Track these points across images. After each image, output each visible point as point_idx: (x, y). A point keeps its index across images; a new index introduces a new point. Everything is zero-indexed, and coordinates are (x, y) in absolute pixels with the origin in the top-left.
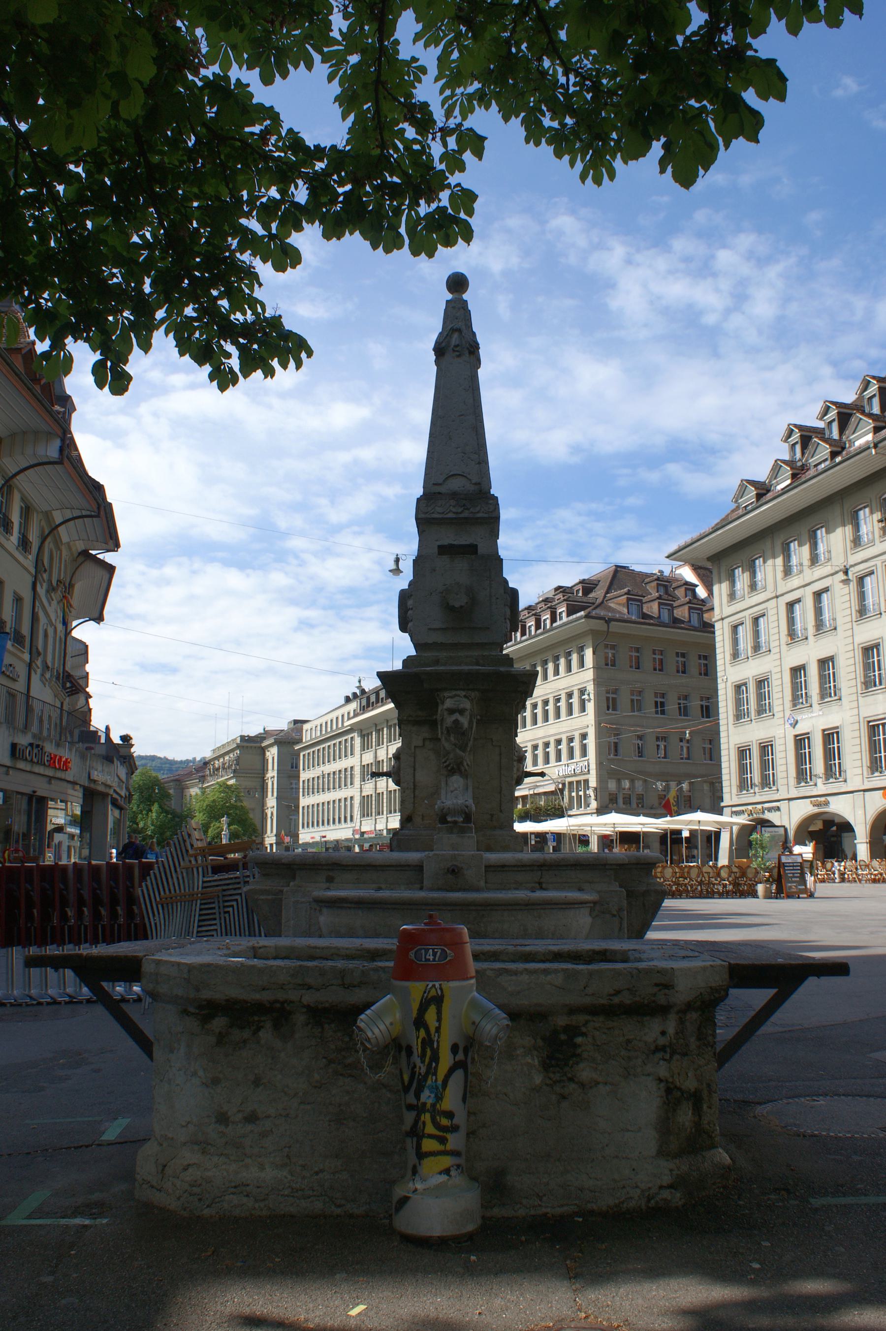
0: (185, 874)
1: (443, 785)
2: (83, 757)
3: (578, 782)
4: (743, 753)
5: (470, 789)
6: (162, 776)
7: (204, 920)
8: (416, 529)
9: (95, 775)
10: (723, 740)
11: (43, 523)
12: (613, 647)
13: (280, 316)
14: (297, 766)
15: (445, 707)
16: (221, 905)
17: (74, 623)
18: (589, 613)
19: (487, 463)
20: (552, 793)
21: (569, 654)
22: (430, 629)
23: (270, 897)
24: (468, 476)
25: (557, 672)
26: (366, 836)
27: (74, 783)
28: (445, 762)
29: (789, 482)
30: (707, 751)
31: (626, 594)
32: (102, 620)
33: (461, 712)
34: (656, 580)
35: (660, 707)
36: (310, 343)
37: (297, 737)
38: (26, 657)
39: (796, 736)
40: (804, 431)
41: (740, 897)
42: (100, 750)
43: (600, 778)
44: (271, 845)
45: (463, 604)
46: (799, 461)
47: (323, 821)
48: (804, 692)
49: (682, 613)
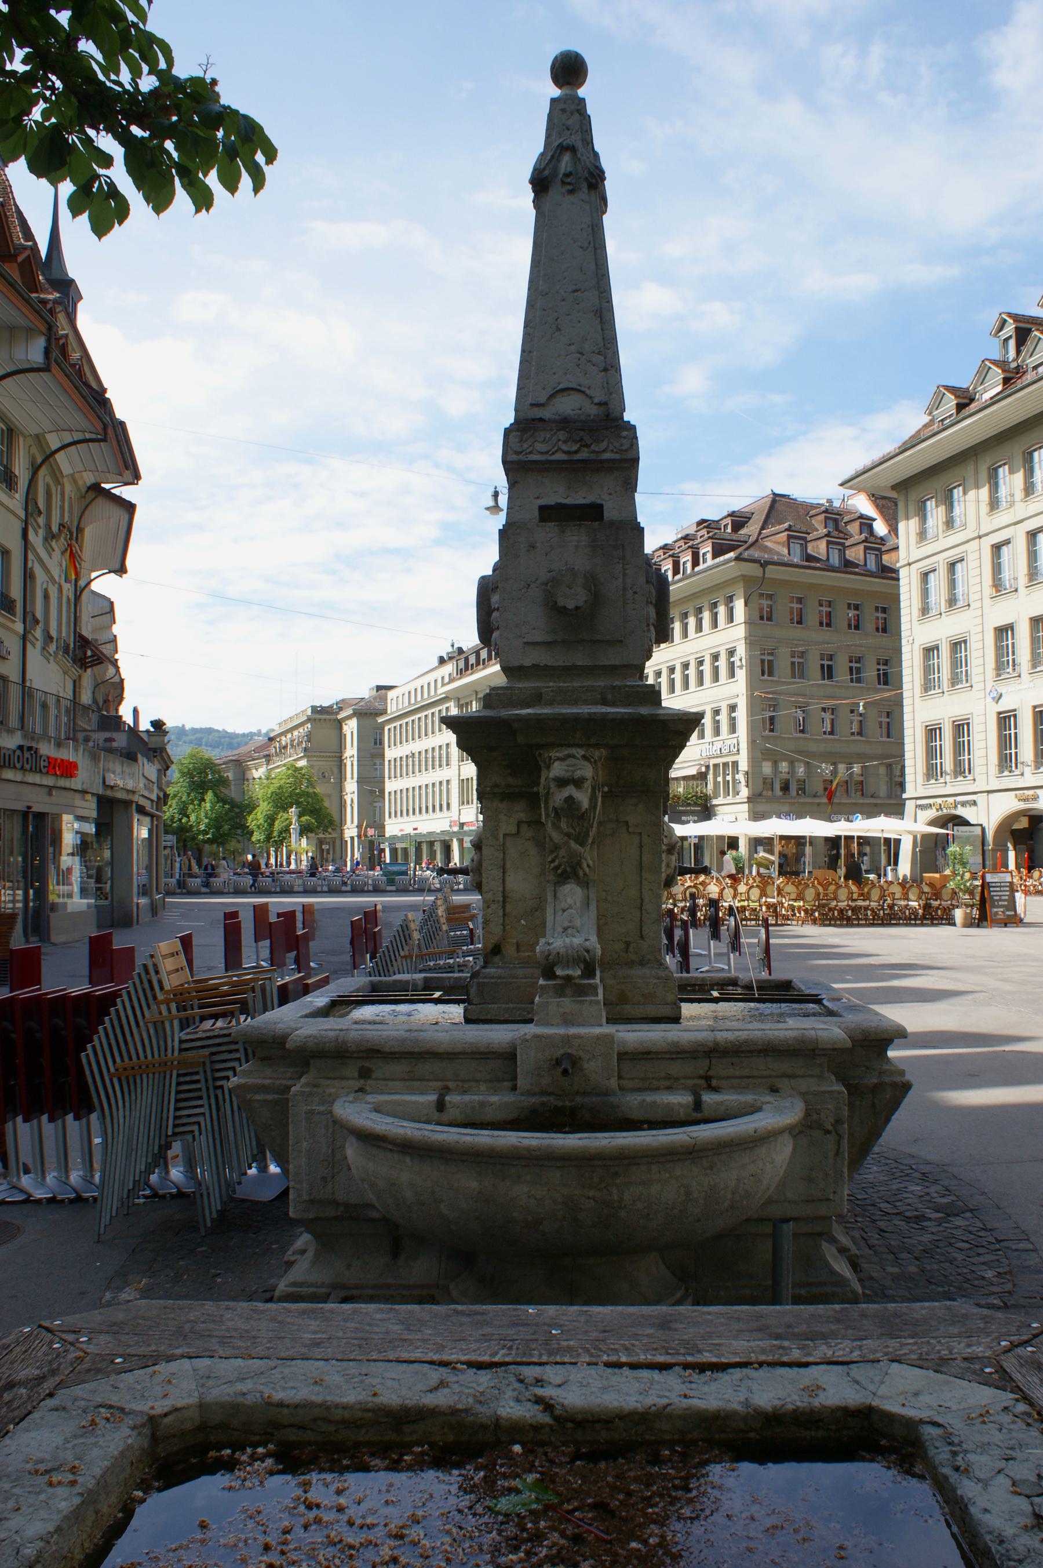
0: (152, 1031)
1: (550, 898)
2: (94, 757)
3: (726, 765)
4: (932, 732)
5: (593, 907)
6: (216, 755)
7: (185, 1100)
8: (505, 478)
9: (112, 779)
10: (907, 717)
11: (34, 450)
12: (770, 597)
13: (214, 82)
14: (381, 743)
15: (551, 775)
16: (210, 1077)
17: (94, 575)
18: (741, 554)
19: (618, 370)
20: (693, 777)
21: (715, 605)
22: (525, 643)
23: (270, 1097)
24: (588, 392)
25: (699, 628)
26: (466, 828)
27: (84, 792)
28: (553, 861)
29: (999, 388)
30: (884, 726)
31: (786, 530)
32: (125, 572)
33: (578, 783)
34: (824, 512)
35: (828, 672)
36: (271, 132)
37: (381, 707)
38: (19, 627)
39: (1000, 713)
40: (1020, 321)
41: (932, 925)
42: (121, 741)
43: (753, 761)
44: (352, 838)
45: (580, 604)
46: (1013, 361)
47: (414, 810)
48: (1010, 658)
49: (855, 554)
